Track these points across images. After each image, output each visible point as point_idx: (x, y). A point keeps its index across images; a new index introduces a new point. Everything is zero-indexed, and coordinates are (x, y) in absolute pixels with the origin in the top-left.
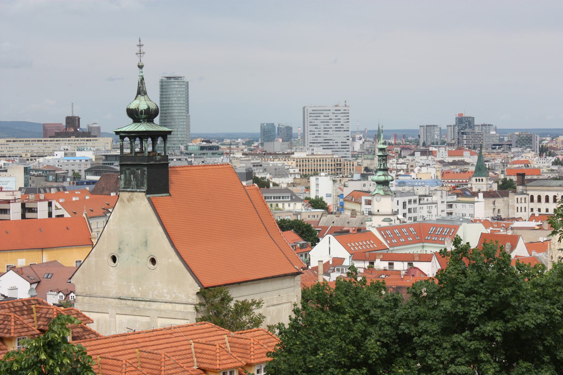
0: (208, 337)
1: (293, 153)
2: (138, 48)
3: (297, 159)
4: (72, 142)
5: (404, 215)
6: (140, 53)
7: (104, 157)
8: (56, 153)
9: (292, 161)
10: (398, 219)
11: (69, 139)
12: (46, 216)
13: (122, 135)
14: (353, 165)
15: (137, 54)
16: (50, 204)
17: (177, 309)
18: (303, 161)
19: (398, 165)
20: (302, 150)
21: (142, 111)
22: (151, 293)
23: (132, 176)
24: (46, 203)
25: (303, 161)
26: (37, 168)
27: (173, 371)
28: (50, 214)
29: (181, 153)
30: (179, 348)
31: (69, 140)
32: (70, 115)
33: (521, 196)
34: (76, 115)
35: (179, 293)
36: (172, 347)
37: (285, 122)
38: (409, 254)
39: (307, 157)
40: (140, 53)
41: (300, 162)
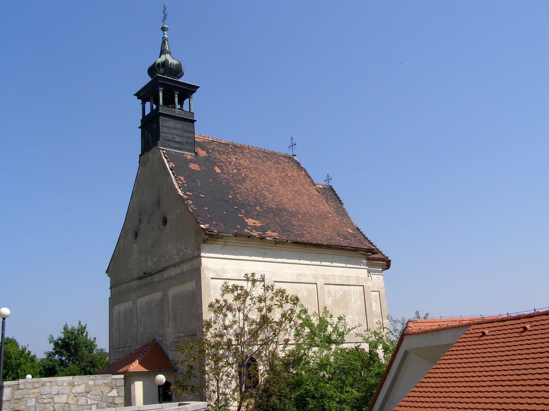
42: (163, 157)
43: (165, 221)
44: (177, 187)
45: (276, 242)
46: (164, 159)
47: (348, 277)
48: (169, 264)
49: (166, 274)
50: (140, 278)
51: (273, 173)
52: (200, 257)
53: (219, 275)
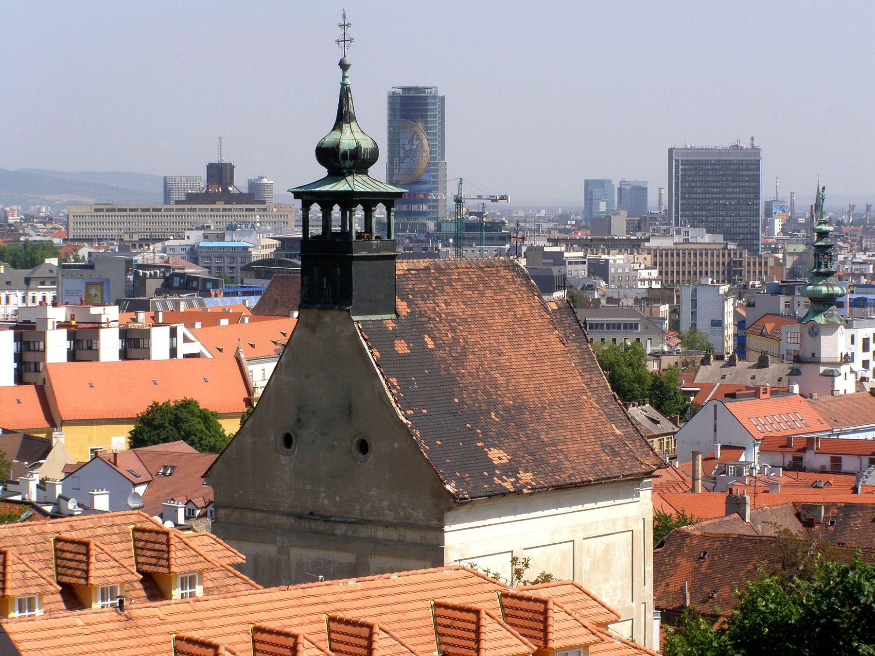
0: (463, 595)
1: (648, 240)
2: (340, 31)
3: (655, 250)
4: (204, 213)
5: (866, 364)
6: (344, 41)
7: (276, 242)
8: (187, 233)
9: (645, 255)
10: (852, 372)
11: (213, 206)
12: (166, 355)
13: (306, 197)
14: (766, 263)
15: (338, 41)
16: (173, 333)
17: (408, 539)
18: (667, 255)
19: (854, 267)
20: (666, 234)
21: (345, 152)
22: (358, 507)
23: (325, 279)
24: (166, 330)
25: (667, 255)
26: (150, 262)
27: (85, 648)
28: (173, 352)
29: (428, 235)
30: (251, 608)
31: (212, 210)
32: (215, 161)
33: (71, 225)
34: (225, 160)
35: (413, 509)
36: (393, 612)
37: (633, 176)
38: (866, 439)
39: (674, 247)
40: (344, 41)
41: (661, 256)
42: (361, 338)
43: (364, 447)
44: (394, 405)
45: (537, 491)
46: (363, 342)
47: (614, 521)
48: (371, 518)
49: (364, 532)
50: (300, 517)
51: (498, 319)
52: (443, 531)
53: (463, 555)
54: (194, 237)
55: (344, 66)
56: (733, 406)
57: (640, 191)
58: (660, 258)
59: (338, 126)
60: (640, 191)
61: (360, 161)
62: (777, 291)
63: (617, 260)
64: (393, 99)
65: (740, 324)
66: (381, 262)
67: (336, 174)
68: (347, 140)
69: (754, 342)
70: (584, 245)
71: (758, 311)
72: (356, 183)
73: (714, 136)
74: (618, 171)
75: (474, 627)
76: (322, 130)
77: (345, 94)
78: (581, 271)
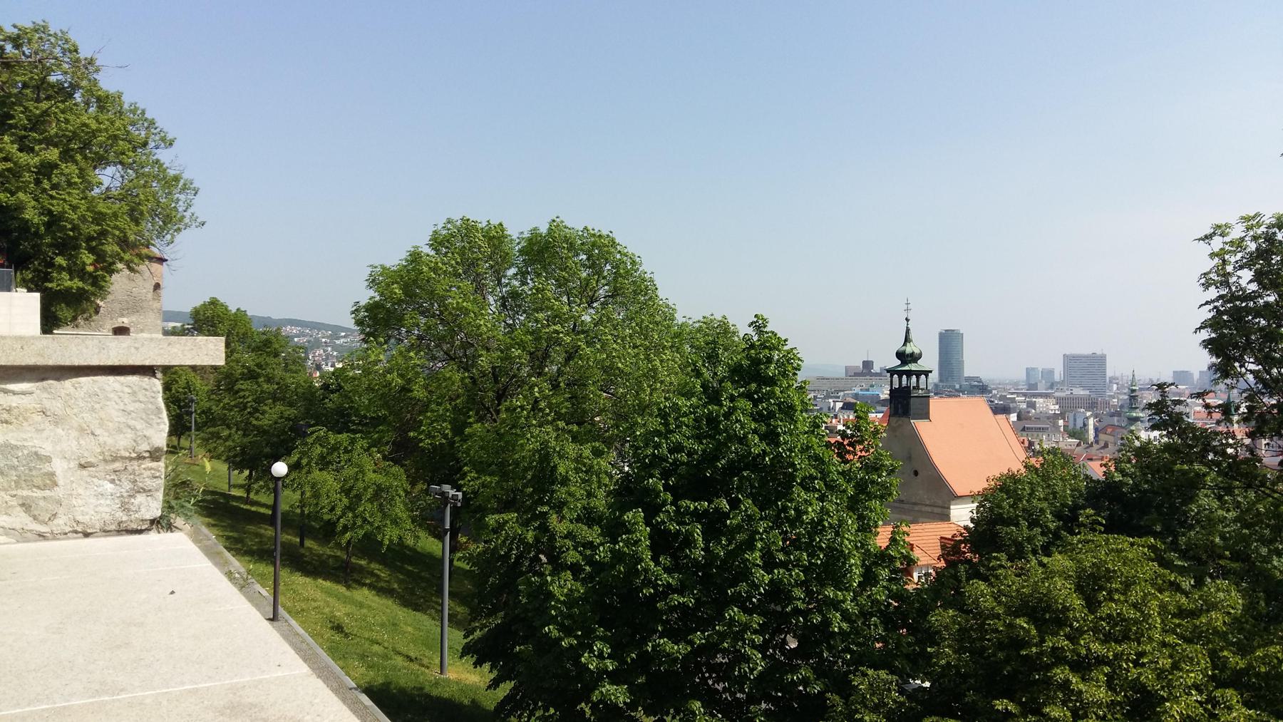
13: (892, 372)
37: (1048, 366)
43: (916, 473)
49: (917, 508)
54: (857, 390)
55: (907, 320)
56: (1090, 463)
57: (1051, 372)
58: (1059, 401)
59: (905, 344)
60: (1051, 372)
61: (914, 358)
62: (1112, 415)
63: (1039, 401)
64: (941, 334)
65: (1096, 430)
66: (111, 378)
67: (904, 363)
68: (909, 349)
69: (1102, 437)
70: (1025, 395)
71: (1104, 424)
72: (913, 367)
73: (1084, 348)
74: (1041, 364)
75: (270, 501)
76: (898, 345)
77: (908, 331)
78: (1024, 406)
